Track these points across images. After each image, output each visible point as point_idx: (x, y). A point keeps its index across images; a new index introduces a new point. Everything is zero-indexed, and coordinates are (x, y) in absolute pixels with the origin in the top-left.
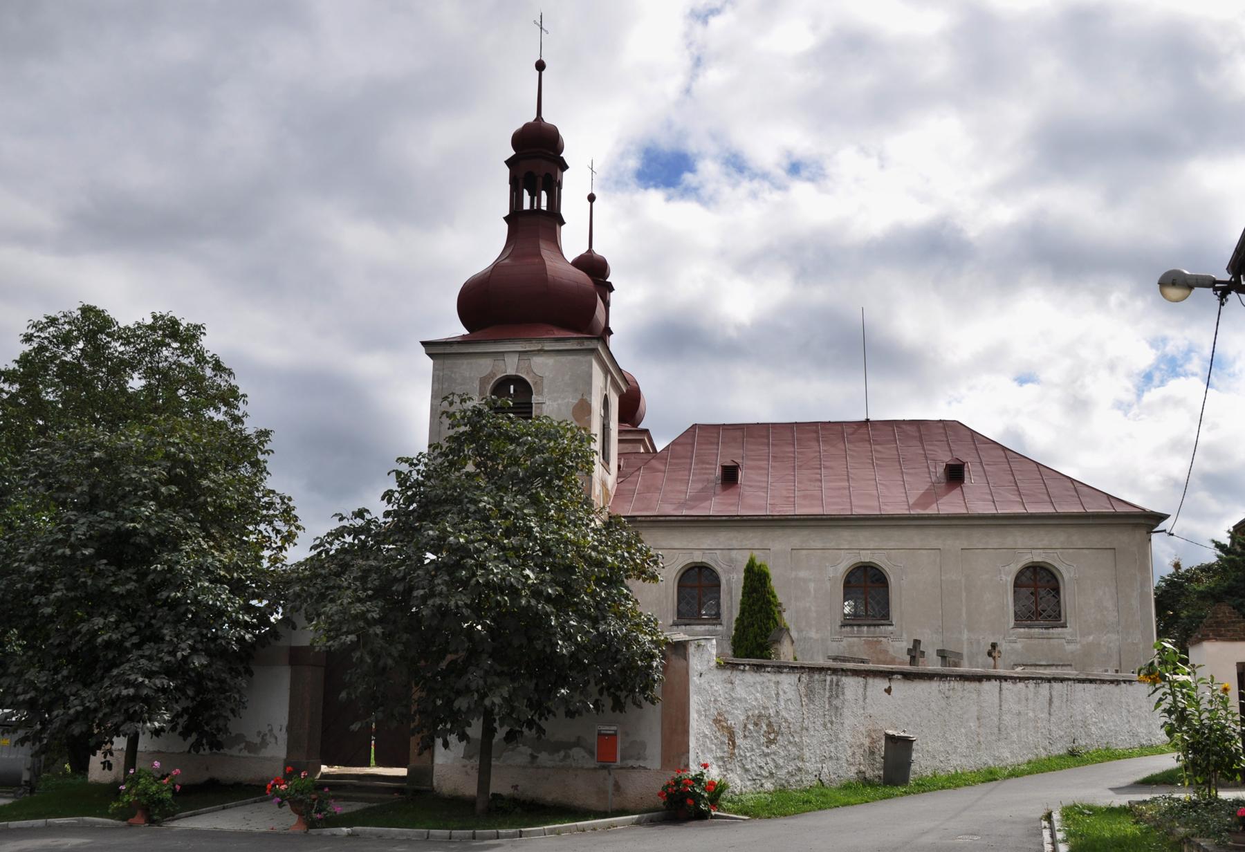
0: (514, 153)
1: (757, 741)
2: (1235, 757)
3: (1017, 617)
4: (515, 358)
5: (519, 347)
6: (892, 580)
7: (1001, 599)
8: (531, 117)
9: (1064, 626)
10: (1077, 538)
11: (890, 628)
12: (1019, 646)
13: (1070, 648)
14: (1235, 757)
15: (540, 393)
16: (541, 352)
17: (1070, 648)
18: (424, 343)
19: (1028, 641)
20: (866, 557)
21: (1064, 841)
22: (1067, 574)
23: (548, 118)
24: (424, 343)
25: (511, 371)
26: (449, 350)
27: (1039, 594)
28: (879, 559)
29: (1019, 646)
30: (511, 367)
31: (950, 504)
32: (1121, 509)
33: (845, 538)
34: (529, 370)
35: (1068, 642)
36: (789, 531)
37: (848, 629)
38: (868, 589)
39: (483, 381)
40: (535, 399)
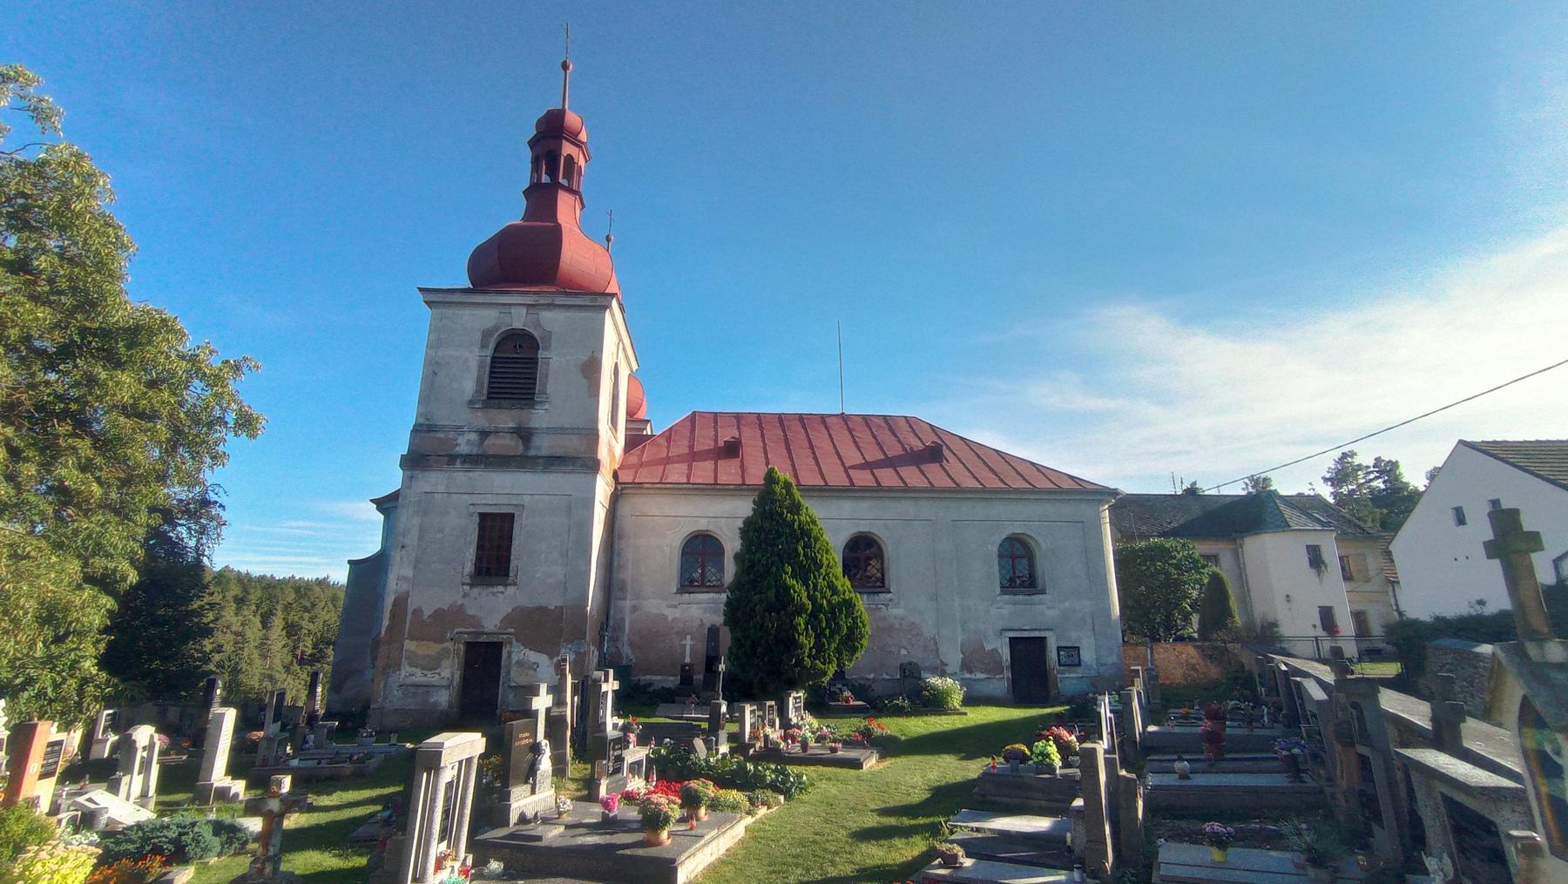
0: (1526, 529)
1: (51, 567)
2: (9, 227)
3: (1002, 587)
4: (524, 310)
5: (529, 300)
6: (889, 551)
7: (986, 570)
9: (1043, 592)
12: (1005, 612)
13: (1050, 613)
14: (9, 227)
15: (547, 348)
16: (550, 306)
17: (1050, 613)
18: (421, 290)
24: (421, 290)
28: (876, 529)
29: (1005, 612)
34: (538, 325)
40: (541, 354)
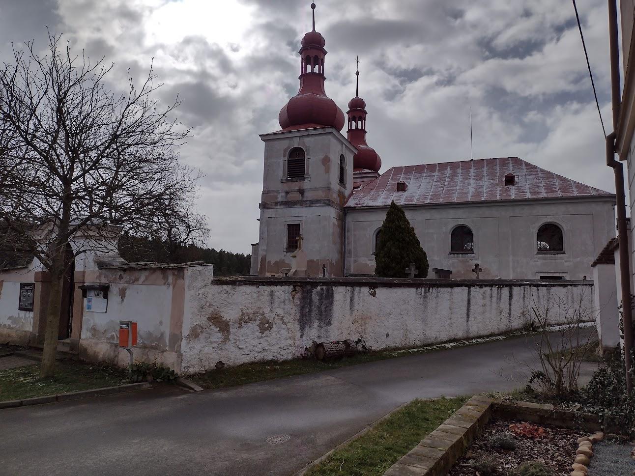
8: (311, 30)
9: (564, 253)
10: (571, 208)
11: (473, 255)
17: (566, 264)
18: (260, 135)
19: (544, 261)
20: (461, 222)
21: (550, 347)
22: (565, 227)
23: (360, 96)
24: (260, 135)
25: (296, 146)
26: (271, 137)
27: (551, 236)
30: (296, 143)
31: (513, 193)
32: (594, 193)
33: (539, 210)
34: (304, 144)
35: (566, 261)
36: (424, 211)
37: (452, 255)
38: (461, 238)
39: (285, 151)
40: (306, 157)
